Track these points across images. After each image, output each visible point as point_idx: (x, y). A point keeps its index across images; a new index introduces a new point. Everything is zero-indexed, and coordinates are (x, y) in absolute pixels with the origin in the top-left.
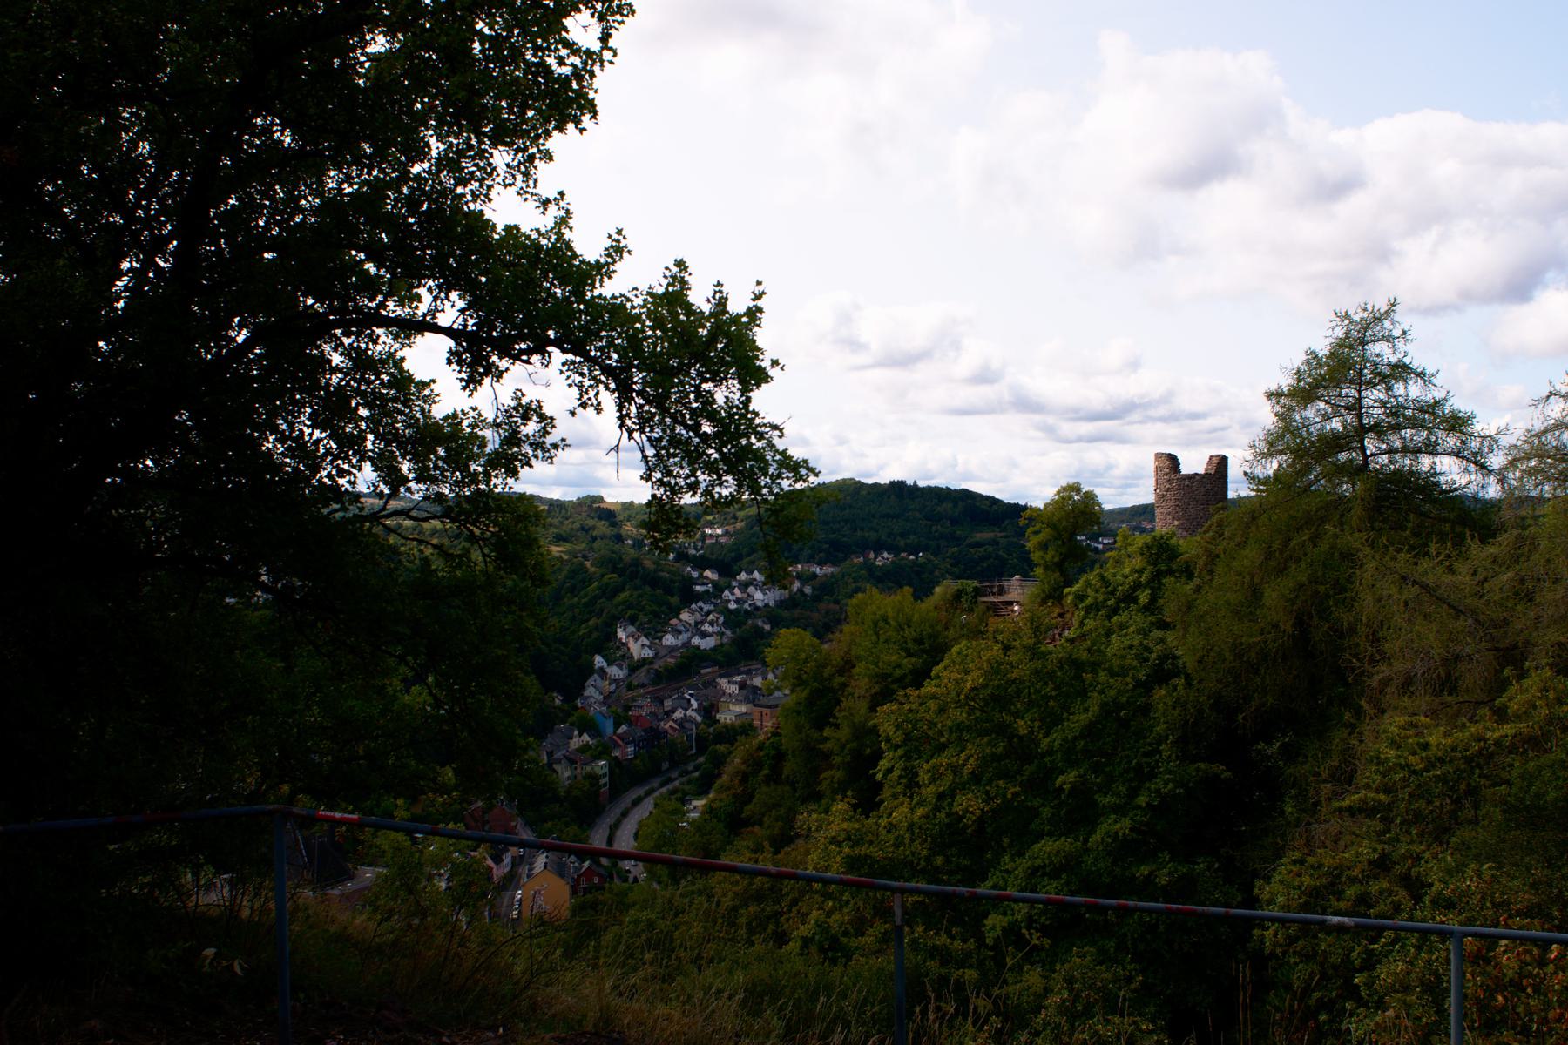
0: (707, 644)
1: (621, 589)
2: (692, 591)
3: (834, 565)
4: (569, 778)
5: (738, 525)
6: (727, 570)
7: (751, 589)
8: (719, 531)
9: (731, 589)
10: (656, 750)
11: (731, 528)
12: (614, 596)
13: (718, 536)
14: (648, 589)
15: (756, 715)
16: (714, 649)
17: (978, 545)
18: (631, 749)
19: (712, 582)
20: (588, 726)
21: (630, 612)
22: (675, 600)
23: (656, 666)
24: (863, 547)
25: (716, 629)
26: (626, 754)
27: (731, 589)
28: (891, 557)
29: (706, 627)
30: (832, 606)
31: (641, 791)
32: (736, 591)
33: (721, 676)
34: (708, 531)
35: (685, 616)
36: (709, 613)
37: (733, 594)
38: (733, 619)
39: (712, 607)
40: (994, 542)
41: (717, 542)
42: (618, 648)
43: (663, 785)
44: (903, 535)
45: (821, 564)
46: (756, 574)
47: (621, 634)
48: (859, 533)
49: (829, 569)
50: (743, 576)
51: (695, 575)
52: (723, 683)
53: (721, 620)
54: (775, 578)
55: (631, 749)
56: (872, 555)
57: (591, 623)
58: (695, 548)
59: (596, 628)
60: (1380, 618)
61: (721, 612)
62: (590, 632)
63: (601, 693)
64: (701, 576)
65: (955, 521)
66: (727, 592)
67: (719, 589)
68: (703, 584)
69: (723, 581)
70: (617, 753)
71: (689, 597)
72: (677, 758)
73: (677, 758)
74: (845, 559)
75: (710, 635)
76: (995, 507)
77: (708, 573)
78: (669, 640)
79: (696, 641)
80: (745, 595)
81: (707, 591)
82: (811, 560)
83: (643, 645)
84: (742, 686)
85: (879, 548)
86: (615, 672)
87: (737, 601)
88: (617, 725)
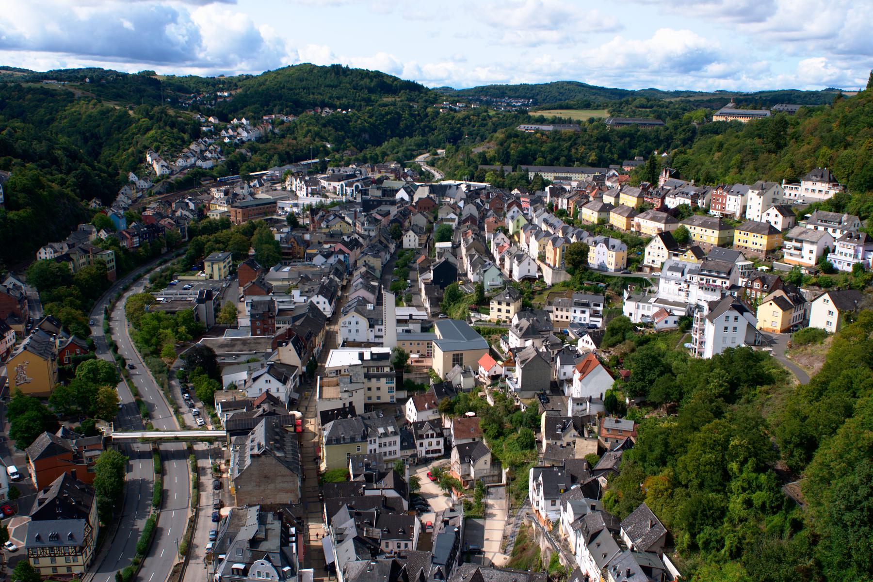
0: (206, 165)
1: (148, 129)
2: (199, 130)
3: (295, 115)
4: (84, 263)
5: (239, 91)
6: (224, 118)
7: (240, 130)
8: (226, 94)
9: (226, 130)
10: (156, 240)
11: (233, 93)
12: (145, 133)
13: (225, 97)
14: (168, 128)
15: (233, 214)
16: (211, 169)
17: (385, 105)
18: (136, 239)
19: (214, 125)
20: (107, 225)
21: (155, 144)
22: (186, 137)
23: (169, 180)
24: (313, 105)
25: (215, 155)
26: (132, 243)
27: (226, 130)
28: (331, 111)
29: (208, 154)
30: (291, 141)
31: (142, 270)
32: (230, 131)
33: (214, 186)
34: (219, 94)
35: (193, 146)
36: (210, 145)
37: (227, 132)
38: (225, 150)
39: (213, 141)
40: (394, 104)
41: (225, 101)
42: (147, 168)
43: (160, 265)
44: (338, 98)
45: (287, 115)
46: (244, 121)
47: (149, 159)
48: (311, 96)
49: (291, 118)
50: (235, 121)
51: (202, 120)
52: (214, 191)
53: (219, 149)
54: (255, 120)
55: (136, 239)
56: (319, 110)
57: (130, 150)
58: (211, 104)
59: (133, 154)
60: (717, 155)
61: (219, 145)
62: (129, 157)
63: (129, 198)
64: (207, 121)
65: (371, 91)
66: (223, 132)
67: (217, 130)
68: (207, 126)
69: (222, 124)
70: (124, 244)
71: (196, 135)
72: (174, 245)
73: (174, 245)
74: (302, 112)
75: (209, 159)
76: (395, 83)
77: (211, 119)
78: (180, 162)
79: (199, 163)
80: (236, 134)
81: (210, 131)
82: (280, 112)
83: (162, 166)
84: (226, 193)
85: (323, 105)
86: (142, 184)
87: (230, 138)
88: (129, 222)
